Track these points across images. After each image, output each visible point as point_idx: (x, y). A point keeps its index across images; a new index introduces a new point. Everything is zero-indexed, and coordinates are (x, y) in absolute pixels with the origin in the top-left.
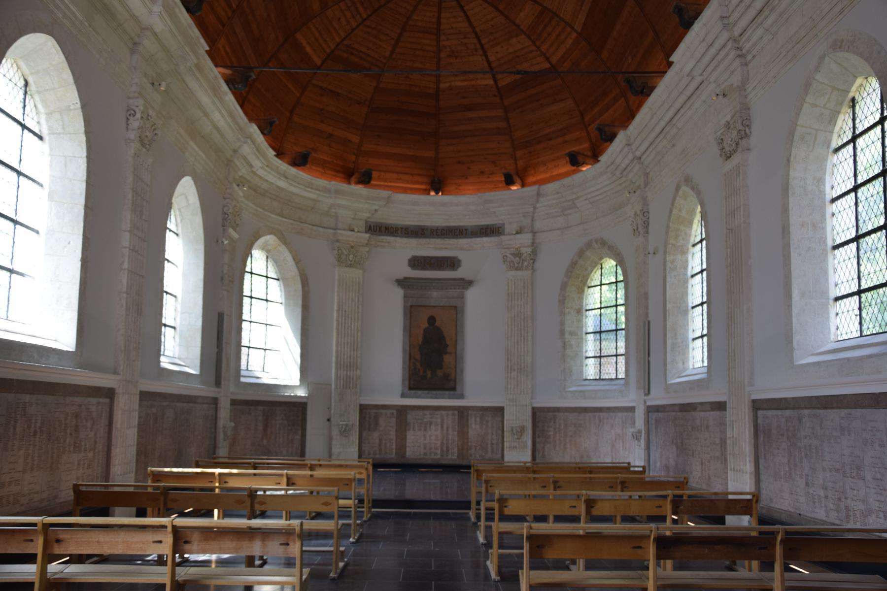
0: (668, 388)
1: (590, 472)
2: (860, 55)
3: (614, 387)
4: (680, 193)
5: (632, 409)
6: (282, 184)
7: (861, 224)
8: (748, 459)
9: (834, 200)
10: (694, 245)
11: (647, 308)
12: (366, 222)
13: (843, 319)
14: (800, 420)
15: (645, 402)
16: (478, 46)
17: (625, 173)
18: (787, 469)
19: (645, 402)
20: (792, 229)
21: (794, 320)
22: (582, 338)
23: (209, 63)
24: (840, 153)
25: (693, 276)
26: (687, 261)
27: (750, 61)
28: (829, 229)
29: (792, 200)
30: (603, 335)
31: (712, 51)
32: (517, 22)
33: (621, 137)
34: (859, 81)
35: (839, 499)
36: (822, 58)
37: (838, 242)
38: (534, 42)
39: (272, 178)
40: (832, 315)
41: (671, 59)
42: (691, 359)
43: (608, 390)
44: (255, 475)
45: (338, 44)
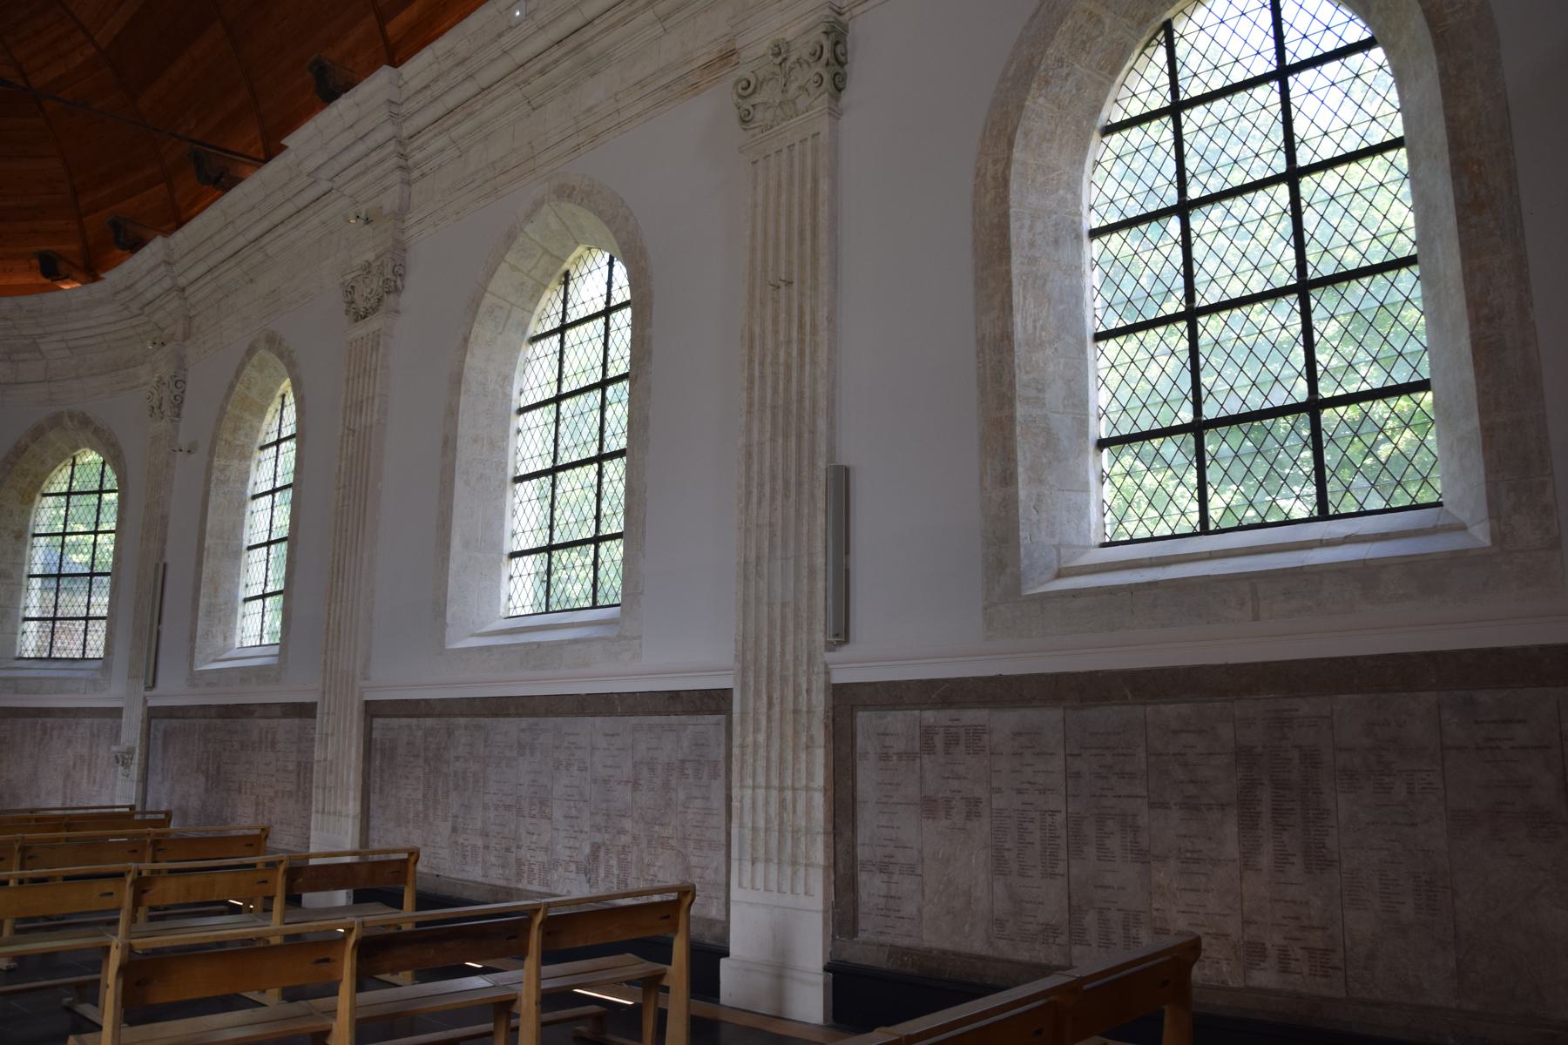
0: (194, 678)
1: (69, 827)
2: (600, 214)
3: (79, 674)
4: (255, 360)
5: (116, 713)
7: (561, 452)
8: (351, 794)
9: (522, 411)
10: (262, 448)
11: (164, 541)
13: (520, 586)
14: (450, 733)
15: (145, 701)
17: (147, 310)
18: (421, 807)
19: (145, 701)
20: (460, 442)
21: (451, 581)
22: (20, 584)
24: (538, 345)
25: (255, 497)
26: (248, 472)
27: (417, 180)
28: (511, 451)
29: (464, 400)
30: (64, 582)
31: (361, 148)
33: (155, 248)
34: (580, 250)
35: (508, 850)
36: (538, 205)
37: (523, 472)
40: (505, 578)
41: (284, 142)
42: (238, 631)
43: (66, 679)
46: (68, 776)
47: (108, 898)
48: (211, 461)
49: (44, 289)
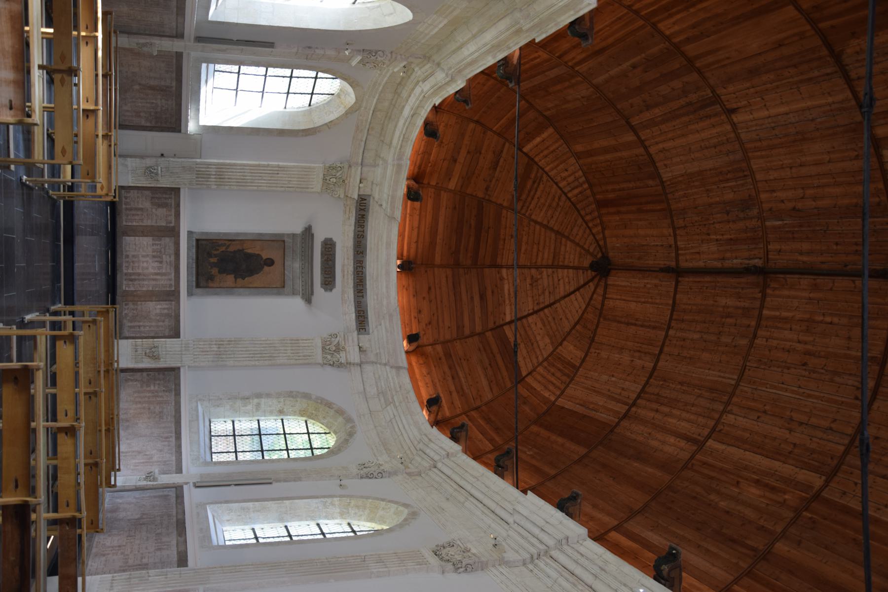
0: (202, 506)
4: (401, 508)
5: (179, 470)
6: (407, 111)
11: (285, 481)
12: (369, 196)
15: (186, 483)
16: (542, 306)
19: (186, 483)
23: (523, 42)
26: (333, 518)
31: (536, 531)
32: (565, 343)
38: (546, 359)
39: (407, 111)
42: (233, 528)
43: (199, 445)
44: (97, 75)
45: (543, 169)
46: (139, 452)
47: (64, 414)
48: (336, 497)
49: (421, 403)
